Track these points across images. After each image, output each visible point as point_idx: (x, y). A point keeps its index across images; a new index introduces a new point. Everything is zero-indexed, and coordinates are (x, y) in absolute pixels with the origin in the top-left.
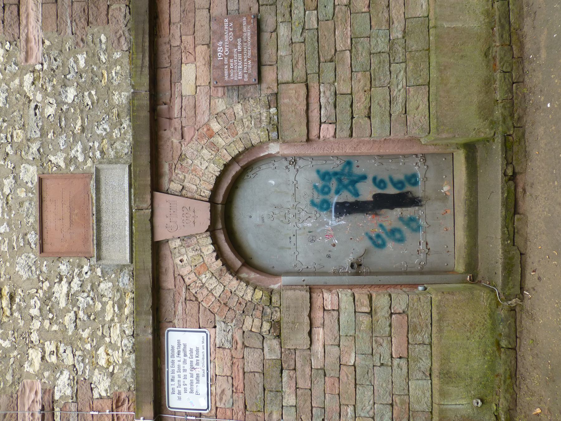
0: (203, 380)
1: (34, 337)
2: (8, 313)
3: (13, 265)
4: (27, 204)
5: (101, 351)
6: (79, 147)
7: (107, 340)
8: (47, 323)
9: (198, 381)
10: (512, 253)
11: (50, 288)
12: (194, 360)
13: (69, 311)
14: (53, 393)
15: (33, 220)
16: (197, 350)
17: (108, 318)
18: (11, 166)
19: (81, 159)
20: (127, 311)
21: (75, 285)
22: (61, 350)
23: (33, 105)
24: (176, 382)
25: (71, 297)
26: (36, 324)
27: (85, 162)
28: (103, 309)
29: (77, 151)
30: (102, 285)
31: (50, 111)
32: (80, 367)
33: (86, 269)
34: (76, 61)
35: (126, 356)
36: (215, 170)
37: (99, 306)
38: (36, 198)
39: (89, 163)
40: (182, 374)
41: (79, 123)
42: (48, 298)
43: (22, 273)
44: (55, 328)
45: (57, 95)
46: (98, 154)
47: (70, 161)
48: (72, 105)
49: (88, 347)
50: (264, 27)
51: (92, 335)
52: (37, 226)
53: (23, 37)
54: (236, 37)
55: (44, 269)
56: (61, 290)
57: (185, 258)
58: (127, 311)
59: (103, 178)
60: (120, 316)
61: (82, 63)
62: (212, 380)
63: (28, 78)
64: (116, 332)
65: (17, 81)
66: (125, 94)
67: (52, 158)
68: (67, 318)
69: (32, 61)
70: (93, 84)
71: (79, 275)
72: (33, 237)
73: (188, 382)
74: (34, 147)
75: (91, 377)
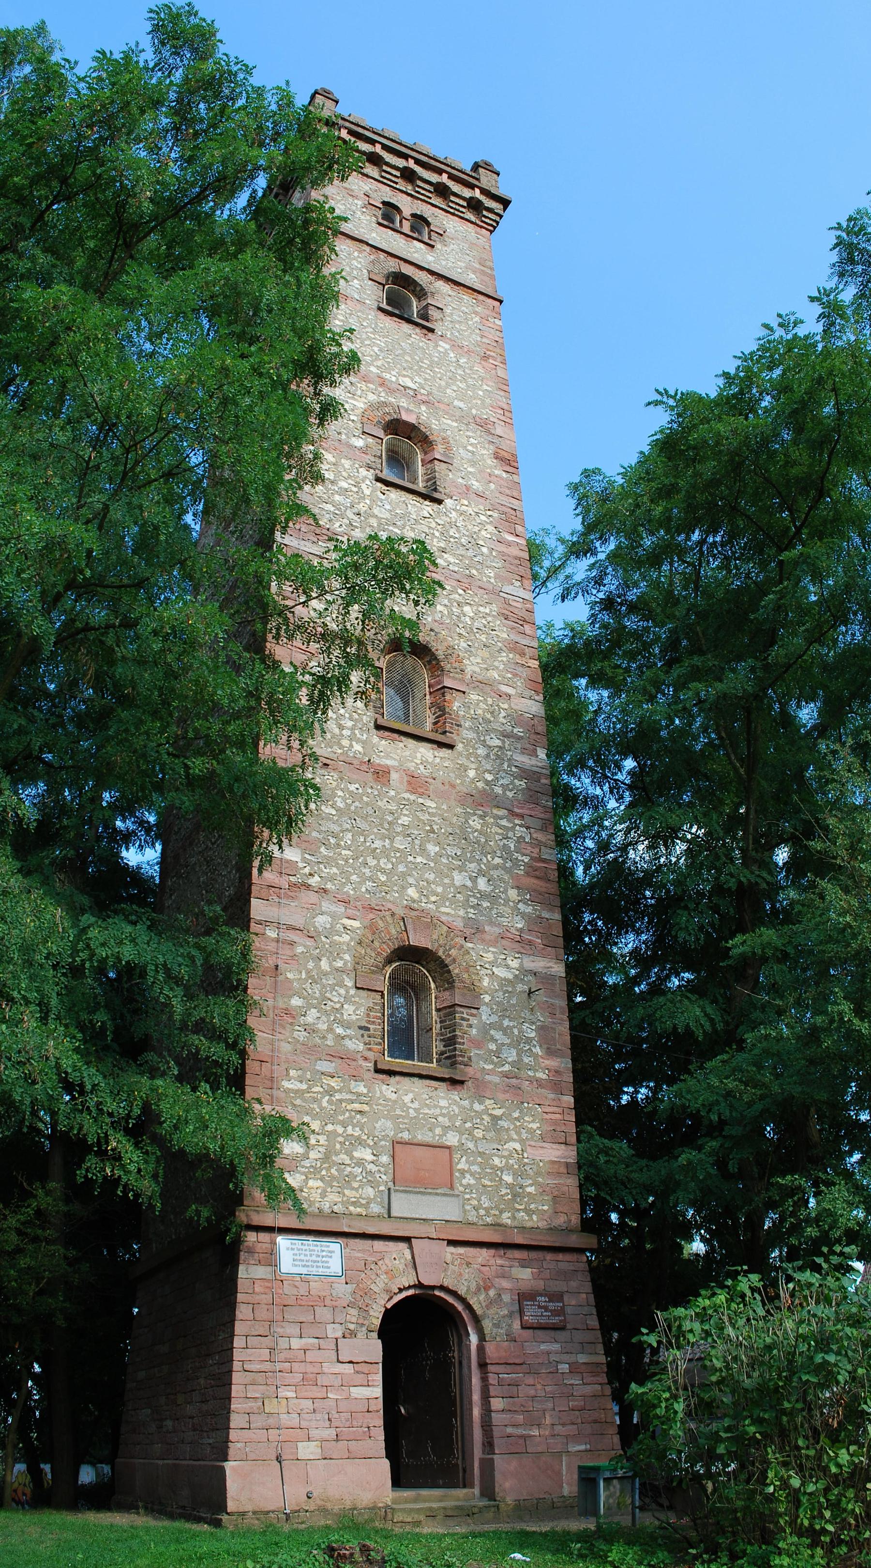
0: (304, 1271)
1: (330, 1127)
2: (349, 1107)
3: (386, 1117)
4: (431, 1134)
5: (319, 1183)
6: (472, 1182)
7: (329, 1190)
8: (341, 1139)
9: (304, 1266)
10: (92, 1104)
11: (369, 1145)
12: (320, 1264)
13: (351, 1159)
14: (505, 979)
15: (419, 1138)
16: (329, 1268)
17: (347, 1192)
18: (457, 1124)
19: (464, 1182)
20: (352, 1208)
21: (371, 1167)
22: (321, 1149)
23: (500, 1147)
24: (300, 1247)
25: (360, 1163)
26: (340, 1130)
27: (461, 1185)
28: (353, 1189)
29: (469, 1180)
30: (371, 1189)
31: (497, 1161)
32: (307, 1163)
33: (384, 1177)
34: (531, 1185)
35: (317, 1205)
36: (462, 1291)
37: (356, 1185)
38: (435, 1142)
39: (461, 1189)
40: (308, 1253)
41: (489, 1183)
42: (361, 1143)
43: (380, 1123)
44: (338, 1146)
45: (508, 1168)
46: (467, 1196)
47: (463, 1172)
48: (501, 1179)
49: (324, 1172)
50: (558, 1332)
51: (333, 1178)
52: (415, 1141)
53: (544, 1145)
54: (551, 1311)
55: (383, 1143)
56: (366, 1154)
57: (397, 1262)
58: (352, 1208)
59: (453, 1199)
60: (348, 1202)
61: (529, 1189)
62: (305, 1279)
63: (518, 1146)
64: (333, 1197)
65: (515, 1137)
66: (509, 1222)
67: (464, 1159)
68: (345, 1156)
69: (529, 1149)
70: (515, 1196)
71: (379, 1171)
72: (406, 1136)
73: (302, 1257)
74: (471, 1145)
75: (299, 1172)
